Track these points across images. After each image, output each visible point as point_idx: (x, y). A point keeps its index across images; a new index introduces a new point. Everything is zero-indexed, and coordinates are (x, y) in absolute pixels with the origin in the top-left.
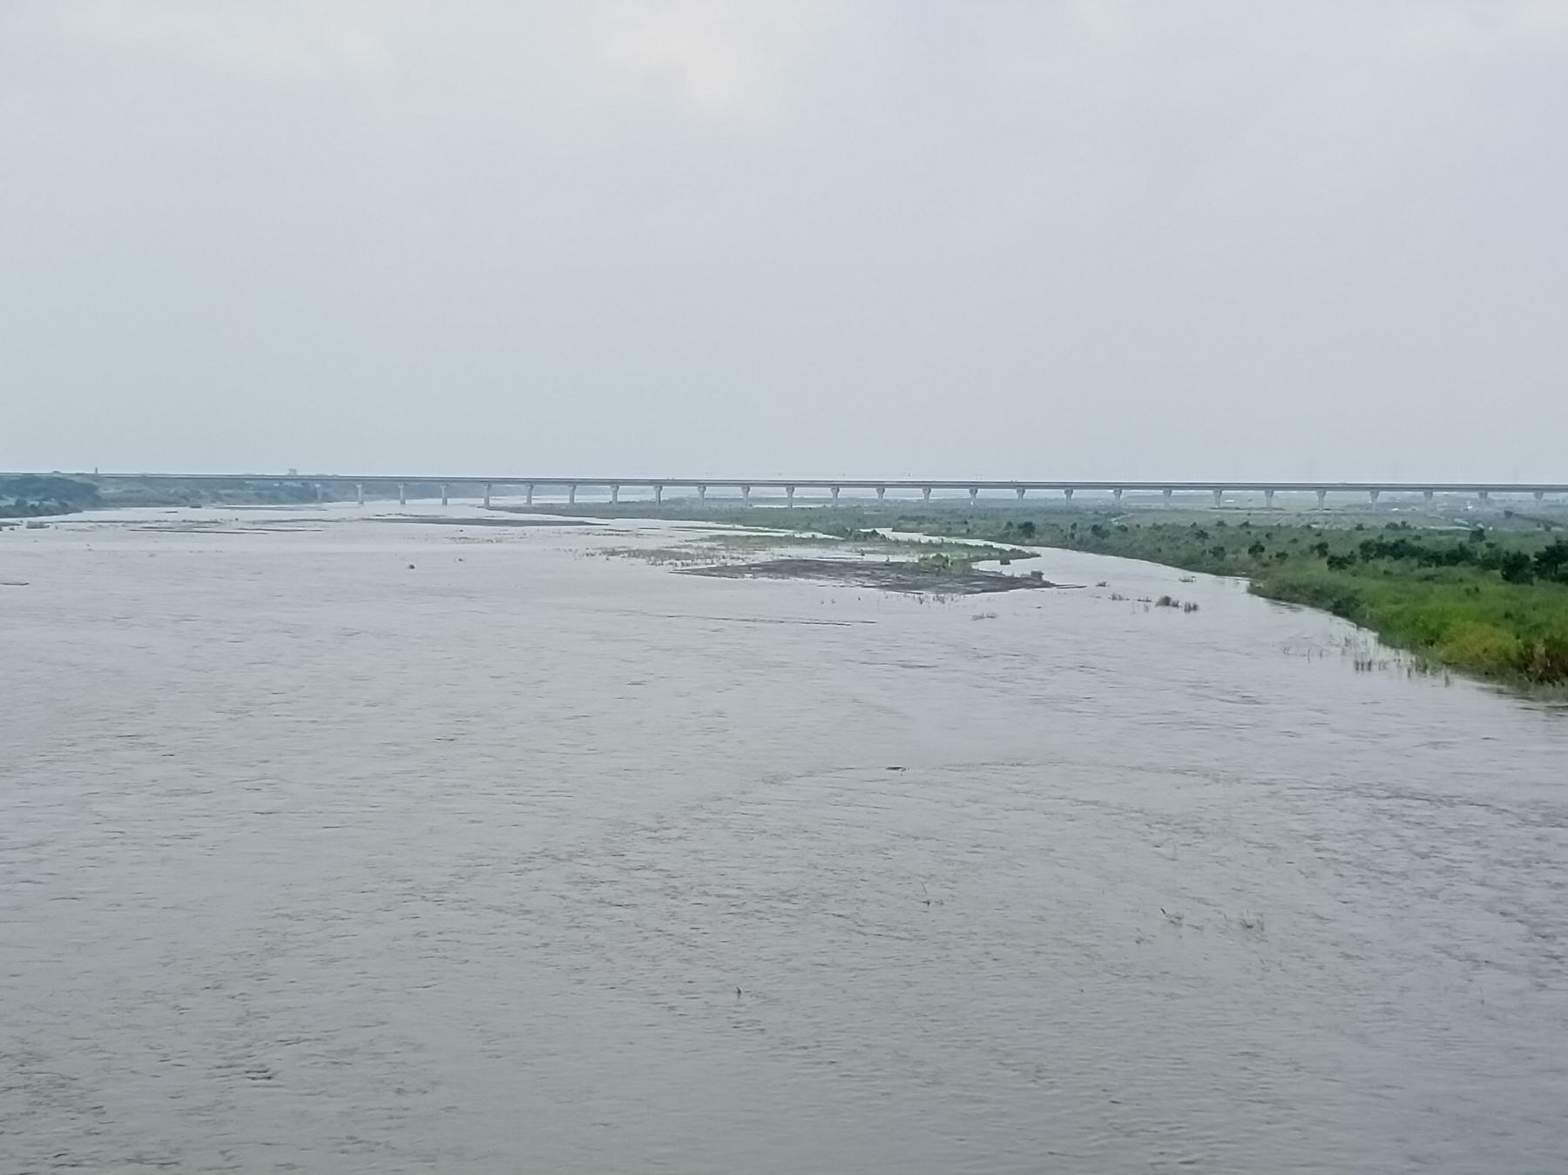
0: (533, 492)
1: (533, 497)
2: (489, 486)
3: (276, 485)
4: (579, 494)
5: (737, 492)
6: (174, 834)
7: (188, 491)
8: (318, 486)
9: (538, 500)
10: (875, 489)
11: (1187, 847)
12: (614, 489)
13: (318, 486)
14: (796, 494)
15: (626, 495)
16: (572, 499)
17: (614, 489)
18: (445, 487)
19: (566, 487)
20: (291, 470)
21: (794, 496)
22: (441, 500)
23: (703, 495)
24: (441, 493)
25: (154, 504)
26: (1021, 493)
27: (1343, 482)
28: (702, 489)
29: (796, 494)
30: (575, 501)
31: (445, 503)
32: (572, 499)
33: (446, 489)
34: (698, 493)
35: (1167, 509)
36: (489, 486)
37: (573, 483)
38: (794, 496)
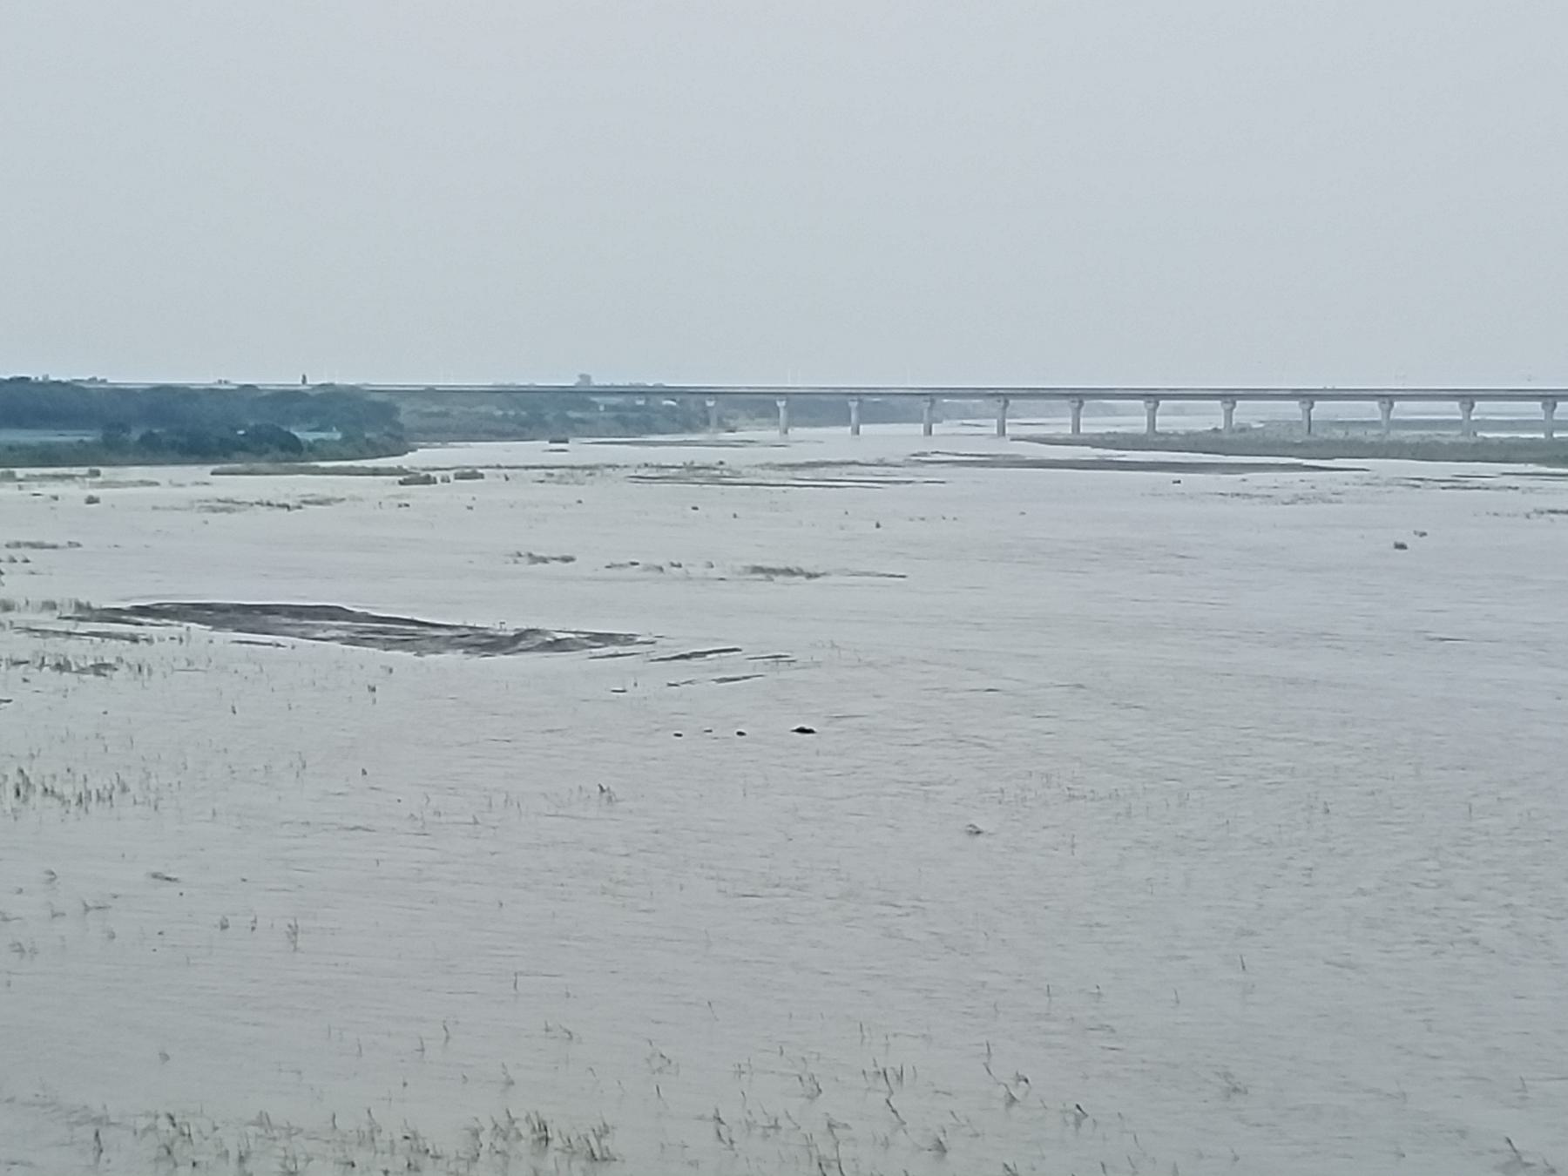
0: (1082, 412)
1: (1007, 421)
2: (932, 401)
3: (641, 402)
4: (1165, 414)
5: (1452, 410)
6: (528, 978)
7: (524, 413)
8: (710, 404)
9: (1092, 425)
10: (1539, 404)
11: (375, 786)
12: (1228, 406)
13: (710, 404)
14: (1476, 414)
15: (1171, 420)
16: (1152, 423)
17: (1151, 405)
18: (856, 404)
19: (1065, 402)
20: (582, 376)
21: (1392, 417)
22: (849, 429)
23: (1388, 416)
24: (922, 414)
25: (484, 436)
26: (1550, 408)
27: (634, 382)
28: (1387, 406)
29: (1559, 414)
30: (1157, 429)
31: (929, 432)
32: (1152, 423)
33: (859, 408)
34: (1300, 411)
35: (1000, 416)
36: (932, 401)
37: (1078, 397)
38: (1556, 418)
